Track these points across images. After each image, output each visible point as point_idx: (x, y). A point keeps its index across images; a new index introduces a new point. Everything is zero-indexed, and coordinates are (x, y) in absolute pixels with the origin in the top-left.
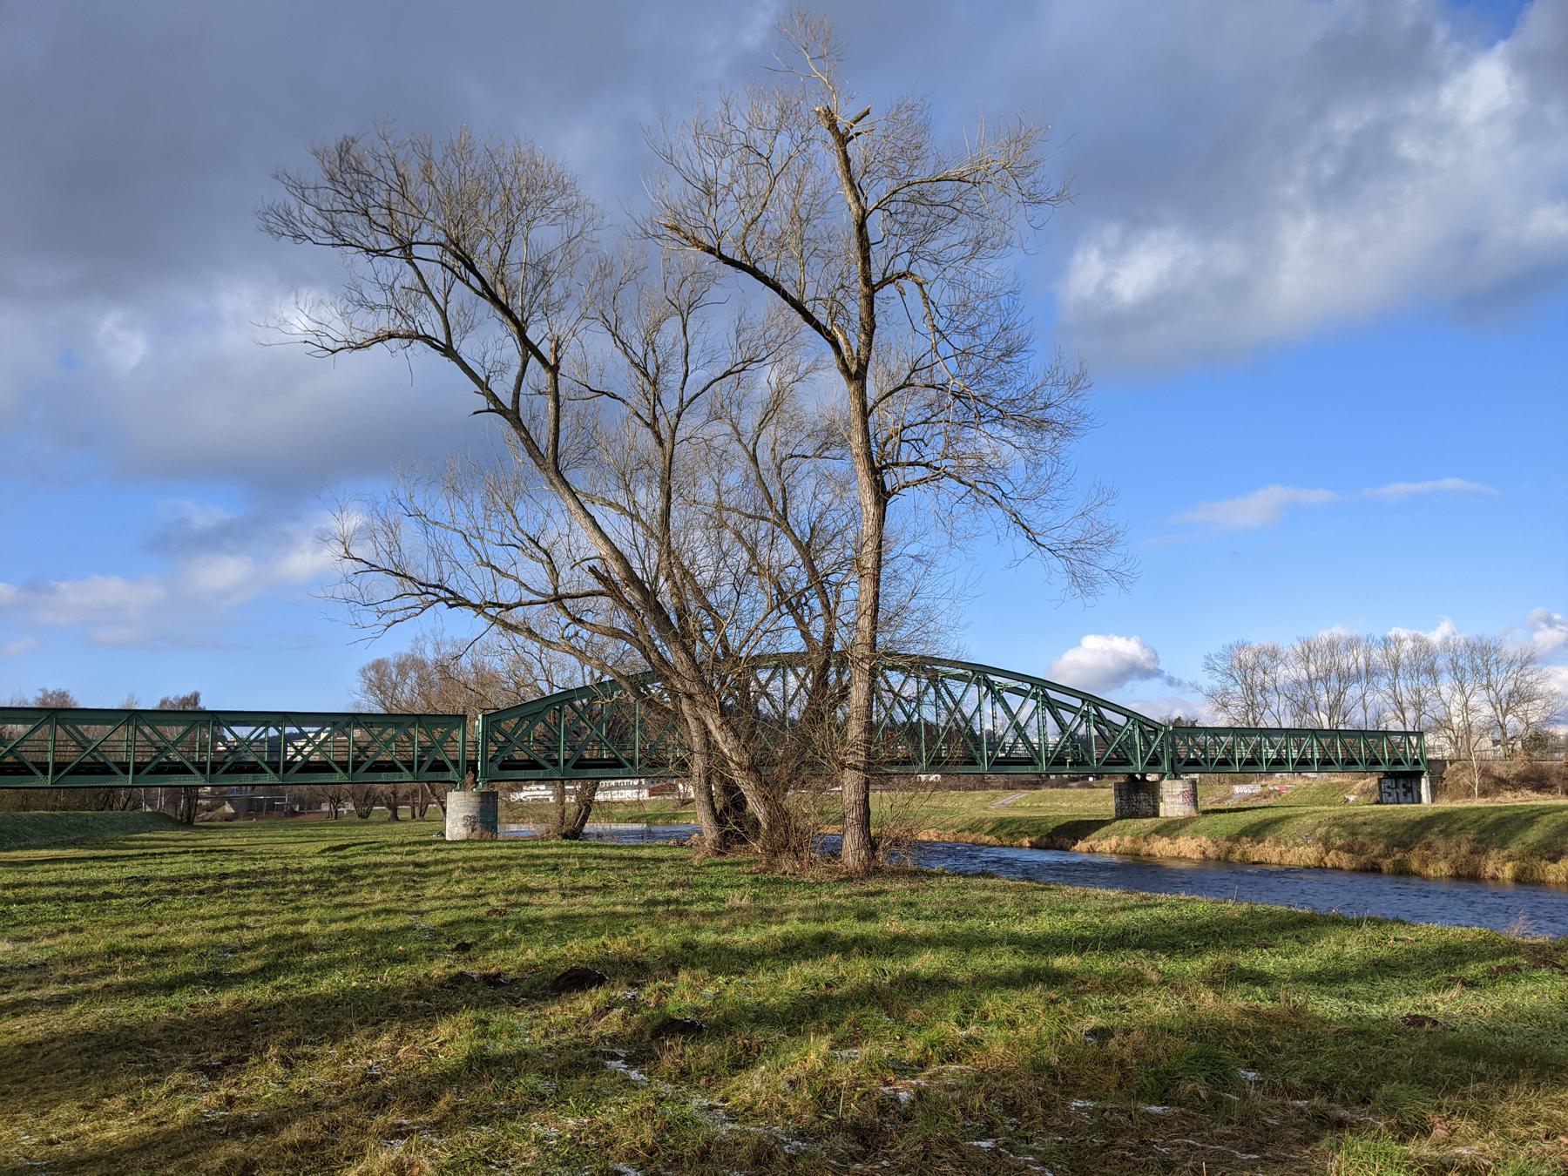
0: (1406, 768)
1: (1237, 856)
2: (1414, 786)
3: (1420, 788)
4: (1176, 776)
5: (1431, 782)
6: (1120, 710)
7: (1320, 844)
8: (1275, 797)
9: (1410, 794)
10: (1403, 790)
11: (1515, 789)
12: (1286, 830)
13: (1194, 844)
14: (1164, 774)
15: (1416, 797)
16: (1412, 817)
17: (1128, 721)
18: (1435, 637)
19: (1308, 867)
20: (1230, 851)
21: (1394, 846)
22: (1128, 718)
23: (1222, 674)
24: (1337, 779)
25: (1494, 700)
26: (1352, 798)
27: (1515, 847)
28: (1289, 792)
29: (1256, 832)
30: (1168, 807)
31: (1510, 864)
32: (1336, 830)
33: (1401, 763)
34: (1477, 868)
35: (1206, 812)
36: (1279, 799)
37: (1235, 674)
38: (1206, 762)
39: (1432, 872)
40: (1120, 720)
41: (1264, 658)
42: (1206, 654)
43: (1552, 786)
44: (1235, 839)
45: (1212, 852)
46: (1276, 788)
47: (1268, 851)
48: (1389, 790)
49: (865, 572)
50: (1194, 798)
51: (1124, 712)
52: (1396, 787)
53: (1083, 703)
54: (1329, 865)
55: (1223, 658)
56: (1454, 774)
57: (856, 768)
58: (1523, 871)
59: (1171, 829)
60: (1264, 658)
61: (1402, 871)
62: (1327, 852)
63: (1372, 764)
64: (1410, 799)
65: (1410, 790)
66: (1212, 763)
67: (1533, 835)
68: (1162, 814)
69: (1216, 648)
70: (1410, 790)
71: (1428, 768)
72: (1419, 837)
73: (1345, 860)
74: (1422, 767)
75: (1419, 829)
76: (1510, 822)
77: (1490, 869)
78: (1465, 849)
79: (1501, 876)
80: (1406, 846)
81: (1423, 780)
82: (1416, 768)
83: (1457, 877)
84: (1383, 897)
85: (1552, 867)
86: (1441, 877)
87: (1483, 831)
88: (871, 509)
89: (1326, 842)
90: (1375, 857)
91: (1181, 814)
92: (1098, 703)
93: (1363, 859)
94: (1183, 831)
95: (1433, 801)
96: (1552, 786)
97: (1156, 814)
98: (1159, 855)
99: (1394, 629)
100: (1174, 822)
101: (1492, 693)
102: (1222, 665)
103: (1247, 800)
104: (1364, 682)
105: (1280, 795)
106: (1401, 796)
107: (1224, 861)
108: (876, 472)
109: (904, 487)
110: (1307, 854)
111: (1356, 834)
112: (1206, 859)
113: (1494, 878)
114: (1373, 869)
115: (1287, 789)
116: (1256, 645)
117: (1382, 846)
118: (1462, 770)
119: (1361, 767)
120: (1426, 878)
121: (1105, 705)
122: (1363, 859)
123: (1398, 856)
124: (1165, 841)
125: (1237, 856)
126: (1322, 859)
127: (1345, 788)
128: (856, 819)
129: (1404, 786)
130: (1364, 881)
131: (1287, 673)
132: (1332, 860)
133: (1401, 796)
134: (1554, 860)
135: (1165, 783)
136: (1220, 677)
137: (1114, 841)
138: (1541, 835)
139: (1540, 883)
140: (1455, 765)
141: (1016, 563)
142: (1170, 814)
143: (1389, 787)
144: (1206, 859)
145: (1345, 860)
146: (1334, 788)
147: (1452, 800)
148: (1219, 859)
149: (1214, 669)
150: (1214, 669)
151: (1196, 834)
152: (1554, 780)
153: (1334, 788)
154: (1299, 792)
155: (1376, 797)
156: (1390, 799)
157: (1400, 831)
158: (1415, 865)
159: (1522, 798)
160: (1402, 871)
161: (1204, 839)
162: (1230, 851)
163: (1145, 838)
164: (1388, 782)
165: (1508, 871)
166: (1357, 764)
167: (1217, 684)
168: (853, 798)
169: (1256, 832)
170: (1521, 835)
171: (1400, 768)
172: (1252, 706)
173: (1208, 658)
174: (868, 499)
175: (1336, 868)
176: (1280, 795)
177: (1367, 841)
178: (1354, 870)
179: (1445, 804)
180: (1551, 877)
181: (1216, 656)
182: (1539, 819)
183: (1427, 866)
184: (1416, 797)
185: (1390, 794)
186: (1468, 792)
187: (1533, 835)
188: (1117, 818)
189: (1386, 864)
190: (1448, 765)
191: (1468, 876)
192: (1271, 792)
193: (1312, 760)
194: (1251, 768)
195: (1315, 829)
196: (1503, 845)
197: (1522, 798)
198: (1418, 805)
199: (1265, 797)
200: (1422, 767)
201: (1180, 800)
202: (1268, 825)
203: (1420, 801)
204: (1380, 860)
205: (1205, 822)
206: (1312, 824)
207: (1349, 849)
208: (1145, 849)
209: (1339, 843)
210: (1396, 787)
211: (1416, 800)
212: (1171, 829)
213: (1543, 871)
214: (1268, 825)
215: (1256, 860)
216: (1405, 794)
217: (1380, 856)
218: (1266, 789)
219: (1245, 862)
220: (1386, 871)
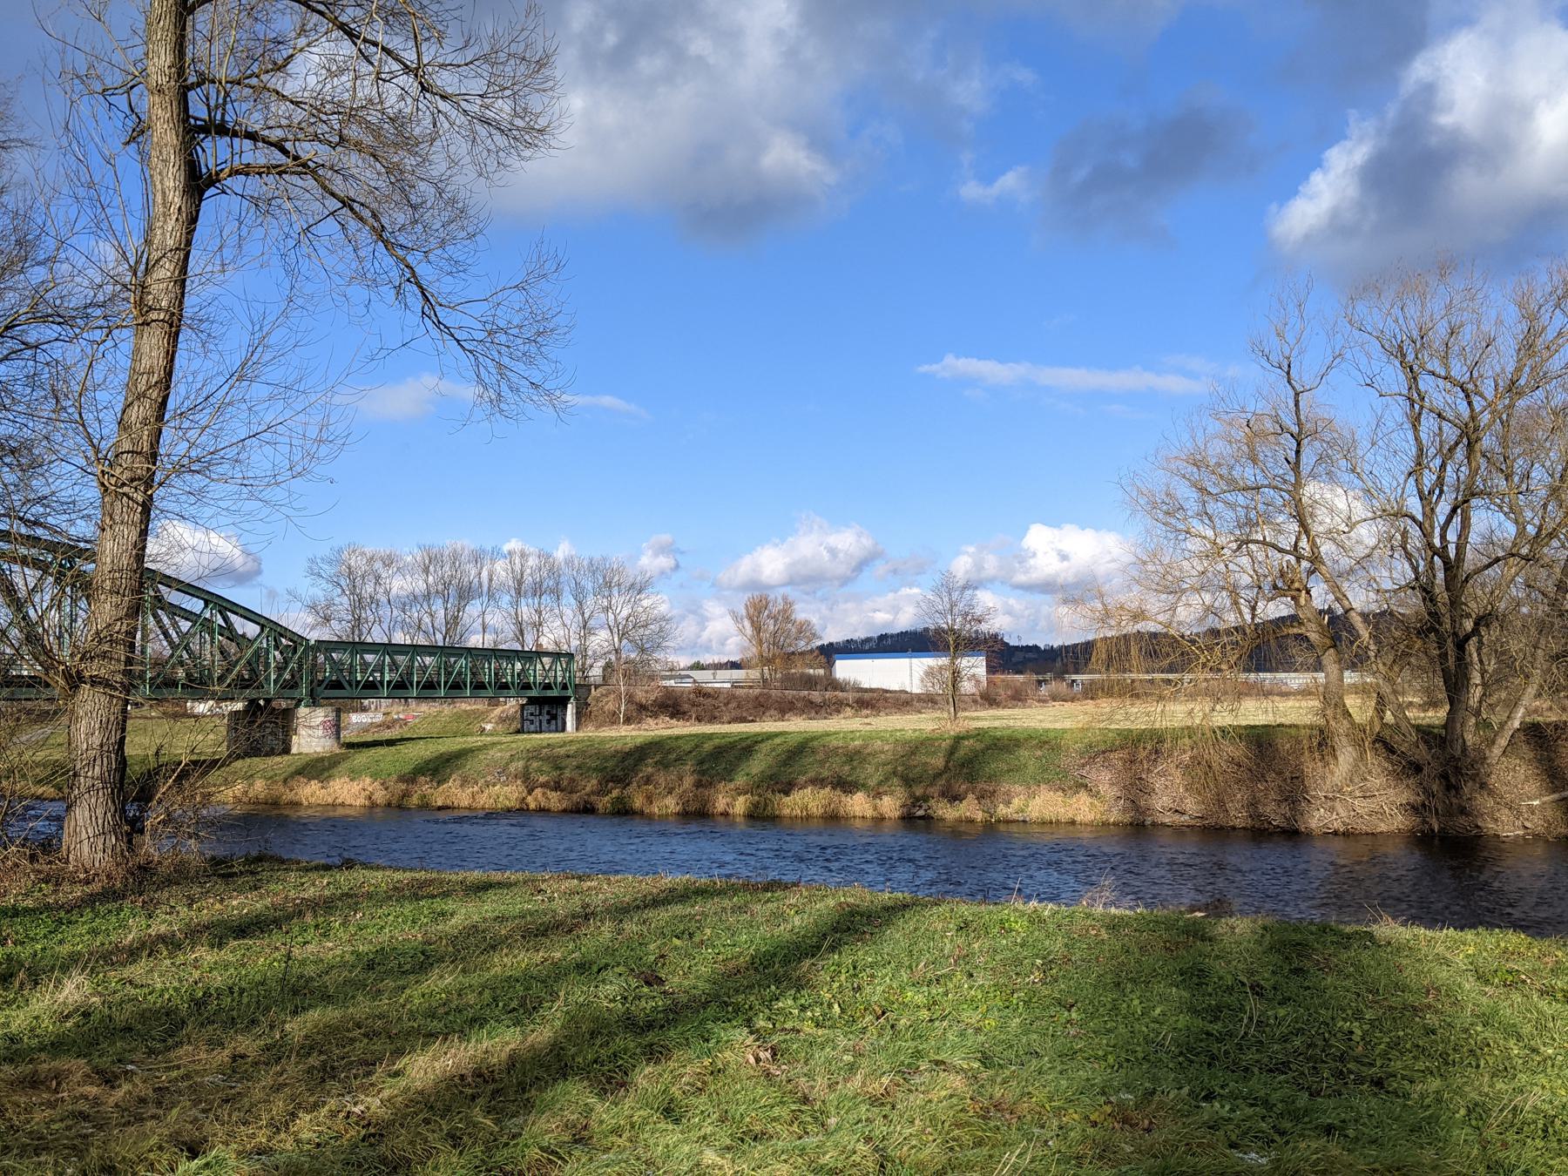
0: (554, 693)
1: (415, 800)
2: (559, 713)
3: (565, 715)
4: (314, 702)
5: (577, 708)
6: (253, 617)
7: (519, 782)
8: (401, 727)
9: (554, 722)
10: (548, 717)
11: (655, 716)
12: (471, 766)
13: (355, 787)
14: (300, 701)
15: (560, 724)
16: (619, 747)
17: (262, 631)
18: (561, 552)
19: (509, 810)
20: (406, 795)
21: (608, 781)
22: (263, 627)
23: (328, 581)
24: (464, 706)
25: (611, 624)
26: (489, 727)
27: (740, 780)
28: (417, 721)
29: (438, 768)
30: (302, 741)
31: (742, 799)
32: (535, 765)
33: (551, 688)
34: (705, 803)
35: (351, 746)
36: (406, 728)
37: (343, 583)
38: (351, 685)
39: (656, 809)
40: (251, 630)
41: (378, 565)
42: (311, 556)
43: (685, 713)
44: (411, 778)
45: (380, 796)
46: (401, 716)
47: (455, 793)
48: (532, 718)
49: (154, 315)
50: (337, 728)
51: (257, 619)
52: (540, 714)
53: (206, 606)
54: (532, 806)
55: (330, 563)
56: (597, 700)
57: (106, 684)
58: (756, 805)
59: (318, 769)
60: (378, 565)
61: (623, 811)
62: (530, 792)
63: (523, 688)
64: (553, 727)
65: (554, 717)
66: (357, 686)
67: (758, 765)
68: (294, 750)
69: (324, 550)
70: (554, 717)
71: (575, 693)
72: (634, 769)
73: (555, 800)
74: (570, 692)
75: (630, 761)
76: (727, 752)
77: (721, 803)
78: (688, 781)
79: (731, 811)
80: (622, 780)
81: (569, 706)
82: (564, 693)
83: (686, 815)
84: (599, 839)
85: (786, 800)
86: (667, 815)
87: (701, 763)
88: (176, 199)
89: (526, 777)
90: (588, 795)
91: (319, 749)
92: (225, 606)
93: (575, 797)
94: (335, 771)
95: (577, 729)
96: (685, 713)
97: (286, 750)
98: (305, 803)
99: (514, 540)
100: (322, 759)
101: (611, 617)
102: (328, 570)
103: (367, 731)
104: (485, 599)
105: (405, 724)
106: (544, 724)
107: (398, 807)
108: (192, 132)
109: (238, 172)
110: (507, 794)
111: (561, 769)
112: (374, 805)
113: (725, 814)
114: (587, 810)
115: (415, 717)
116: (369, 550)
117: (594, 782)
118: (606, 696)
119: (512, 692)
120: (650, 818)
121: (235, 609)
122: (575, 797)
123: (615, 793)
124: (315, 785)
125: (415, 800)
126: (524, 799)
127: (480, 716)
128: (101, 778)
129: (548, 713)
130: (574, 826)
131: (399, 585)
132: (536, 800)
133: (544, 724)
134: (787, 793)
135: (303, 711)
136: (324, 585)
137: (239, 788)
138: (763, 766)
139: (774, 819)
140: (599, 690)
141: (384, 353)
142: (305, 750)
143: (532, 714)
144: (374, 805)
145: (555, 800)
146: (469, 716)
147: (597, 728)
148: (389, 805)
149: (320, 575)
150: (320, 575)
151: (354, 775)
152: (686, 707)
153: (469, 716)
154: (429, 720)
155: (516, 725)
156: (532, 728)
157: (610, 764)
158: (638, 802)
159: (663, 726)
160: (623, 811)
161: (368, 780)
162: (406, 795)
163: (285, 781)
164: (532, 709)
165: (740, 805)
166: (509, 689)
167: (321, 594)
168: (96, 740)
169: (438, 768)
170: (743, 766)
171: (549, 693)
172: (358, 622)
173: (312, 561)
174: (170, 180)
175: (542, 811)
176: (405, 724)
177: (575, 775)
178: (565, 811)
179: (589, 732)
180: (786, 811)
181: (322, 559)
182: (756, 748)
183: (651, 803)
184: (560, 724)
185: (532, 722)
186: (613, 719)
187: (758, 765)
188: (234, 756)
189: (603, 803)
190: (593, 690)
191: (697, 814)
192: (395, 721)
193: (381, 682)
194: (427, 693)
195: (507, 764)
196: (728, 775)
197: (663, 726)
198: (561, 735)
199: (389, 727)
200: (570, 692)
201: (320, 732)
202: (448, 761)
203: (564, 729)
204: (593, 798)
205: (362, 758)
206: (502, 758)
207: (557, 787)
208: (288, 796)
209: (543, 779)
210: (540, 714)
211: (560, 728)
212: (318, 769)
213: (778, 804)
214: (448, 761)
215: (440, 803)
216: (549, 722)
217: (593, 793)
218: (389, 718)
219: (425, 806)
220: (601, 811)
